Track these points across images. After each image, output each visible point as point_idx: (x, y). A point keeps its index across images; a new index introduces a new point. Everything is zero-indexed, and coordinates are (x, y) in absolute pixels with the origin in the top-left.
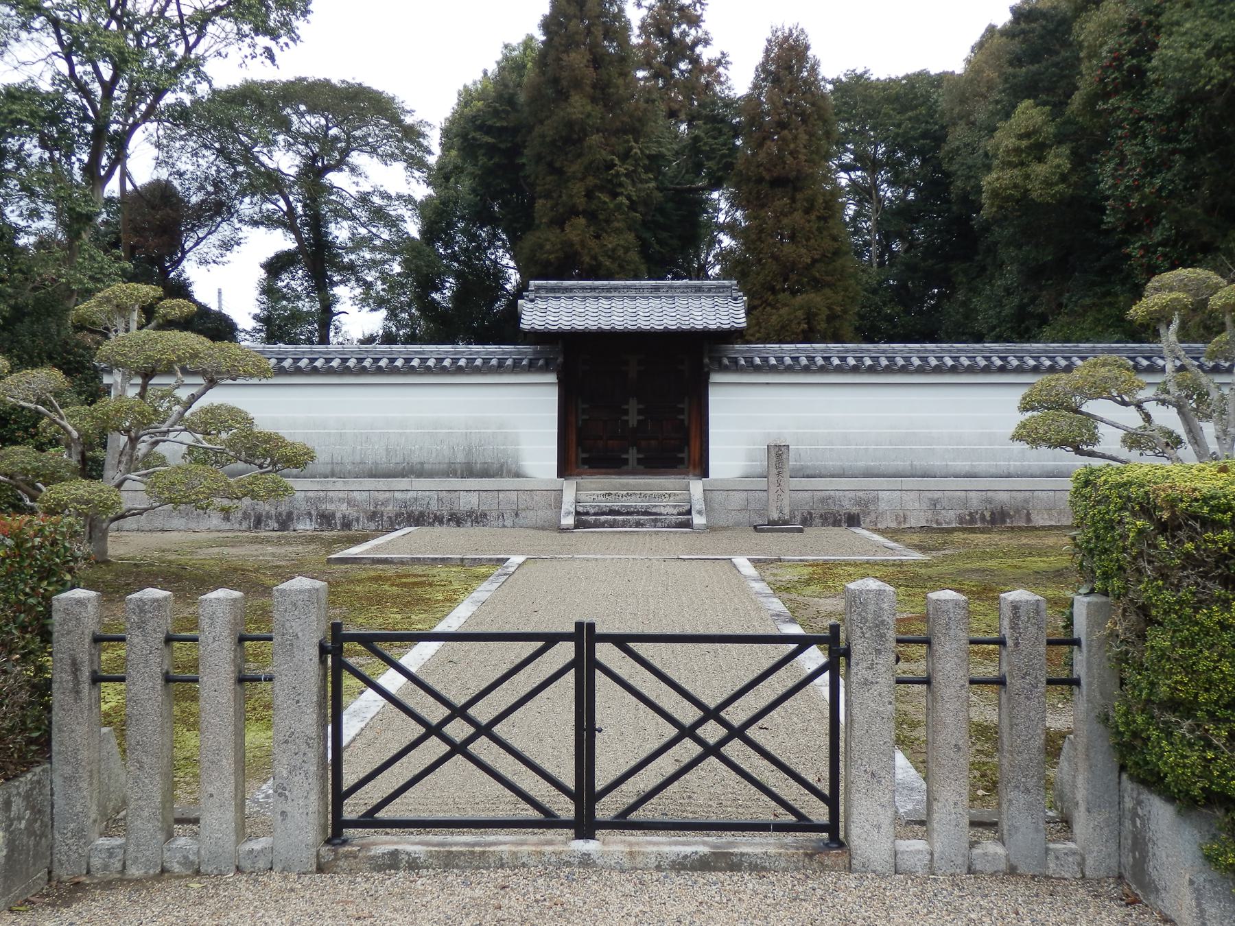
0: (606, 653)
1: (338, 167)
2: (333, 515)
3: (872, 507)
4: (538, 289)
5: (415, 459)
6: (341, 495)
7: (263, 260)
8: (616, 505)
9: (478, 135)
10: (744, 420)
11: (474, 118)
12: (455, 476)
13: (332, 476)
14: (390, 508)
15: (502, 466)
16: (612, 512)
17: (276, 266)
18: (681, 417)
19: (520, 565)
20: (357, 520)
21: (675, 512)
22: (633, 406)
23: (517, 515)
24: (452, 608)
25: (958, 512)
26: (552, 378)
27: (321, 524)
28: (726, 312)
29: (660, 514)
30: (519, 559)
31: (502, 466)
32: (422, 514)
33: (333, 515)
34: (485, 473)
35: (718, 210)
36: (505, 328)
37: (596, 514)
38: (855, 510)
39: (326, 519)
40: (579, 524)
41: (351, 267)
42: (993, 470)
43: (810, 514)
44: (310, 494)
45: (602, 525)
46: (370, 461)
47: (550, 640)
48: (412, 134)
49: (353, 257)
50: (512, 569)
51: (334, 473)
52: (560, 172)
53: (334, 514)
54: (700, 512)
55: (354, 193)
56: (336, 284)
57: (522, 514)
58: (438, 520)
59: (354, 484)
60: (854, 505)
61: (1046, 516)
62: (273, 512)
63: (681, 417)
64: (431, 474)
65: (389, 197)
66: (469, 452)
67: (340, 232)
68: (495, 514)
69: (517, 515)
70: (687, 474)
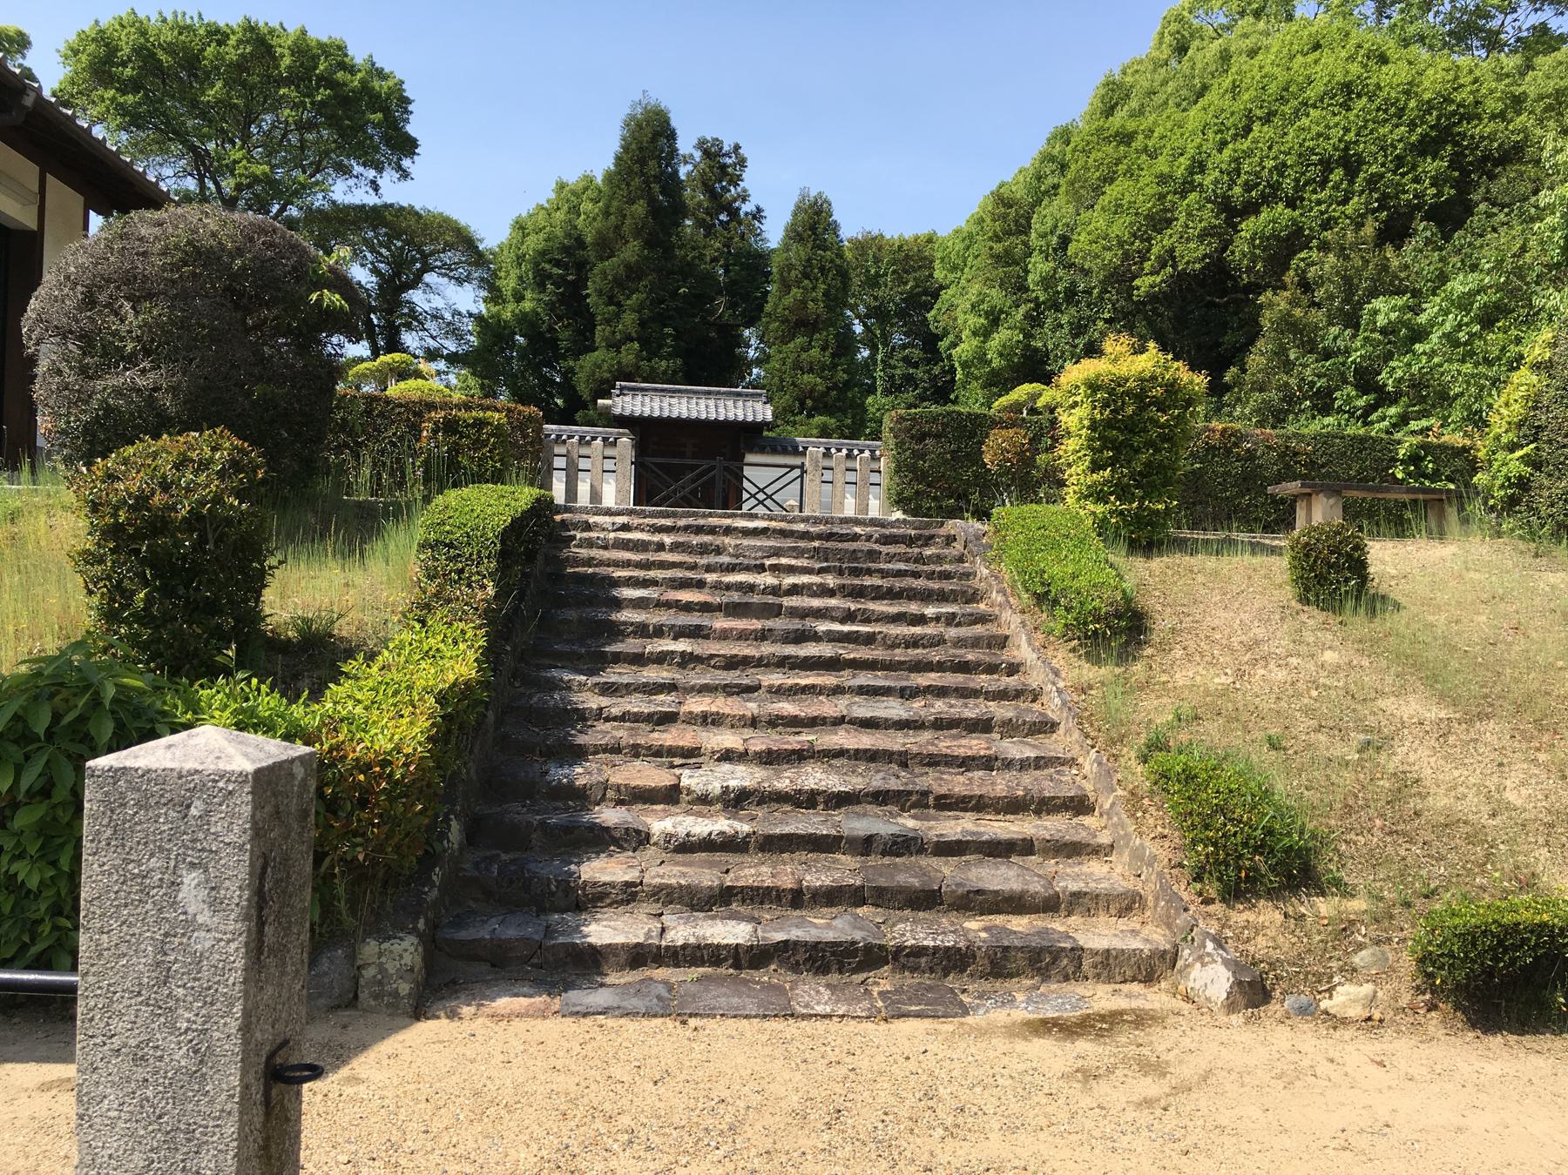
1: (415, 282)
4: (622, 388)
9: (547, 266)
28: (762, 412)
35: (750, 347)
52: (619, 305)
65: (460, 314)
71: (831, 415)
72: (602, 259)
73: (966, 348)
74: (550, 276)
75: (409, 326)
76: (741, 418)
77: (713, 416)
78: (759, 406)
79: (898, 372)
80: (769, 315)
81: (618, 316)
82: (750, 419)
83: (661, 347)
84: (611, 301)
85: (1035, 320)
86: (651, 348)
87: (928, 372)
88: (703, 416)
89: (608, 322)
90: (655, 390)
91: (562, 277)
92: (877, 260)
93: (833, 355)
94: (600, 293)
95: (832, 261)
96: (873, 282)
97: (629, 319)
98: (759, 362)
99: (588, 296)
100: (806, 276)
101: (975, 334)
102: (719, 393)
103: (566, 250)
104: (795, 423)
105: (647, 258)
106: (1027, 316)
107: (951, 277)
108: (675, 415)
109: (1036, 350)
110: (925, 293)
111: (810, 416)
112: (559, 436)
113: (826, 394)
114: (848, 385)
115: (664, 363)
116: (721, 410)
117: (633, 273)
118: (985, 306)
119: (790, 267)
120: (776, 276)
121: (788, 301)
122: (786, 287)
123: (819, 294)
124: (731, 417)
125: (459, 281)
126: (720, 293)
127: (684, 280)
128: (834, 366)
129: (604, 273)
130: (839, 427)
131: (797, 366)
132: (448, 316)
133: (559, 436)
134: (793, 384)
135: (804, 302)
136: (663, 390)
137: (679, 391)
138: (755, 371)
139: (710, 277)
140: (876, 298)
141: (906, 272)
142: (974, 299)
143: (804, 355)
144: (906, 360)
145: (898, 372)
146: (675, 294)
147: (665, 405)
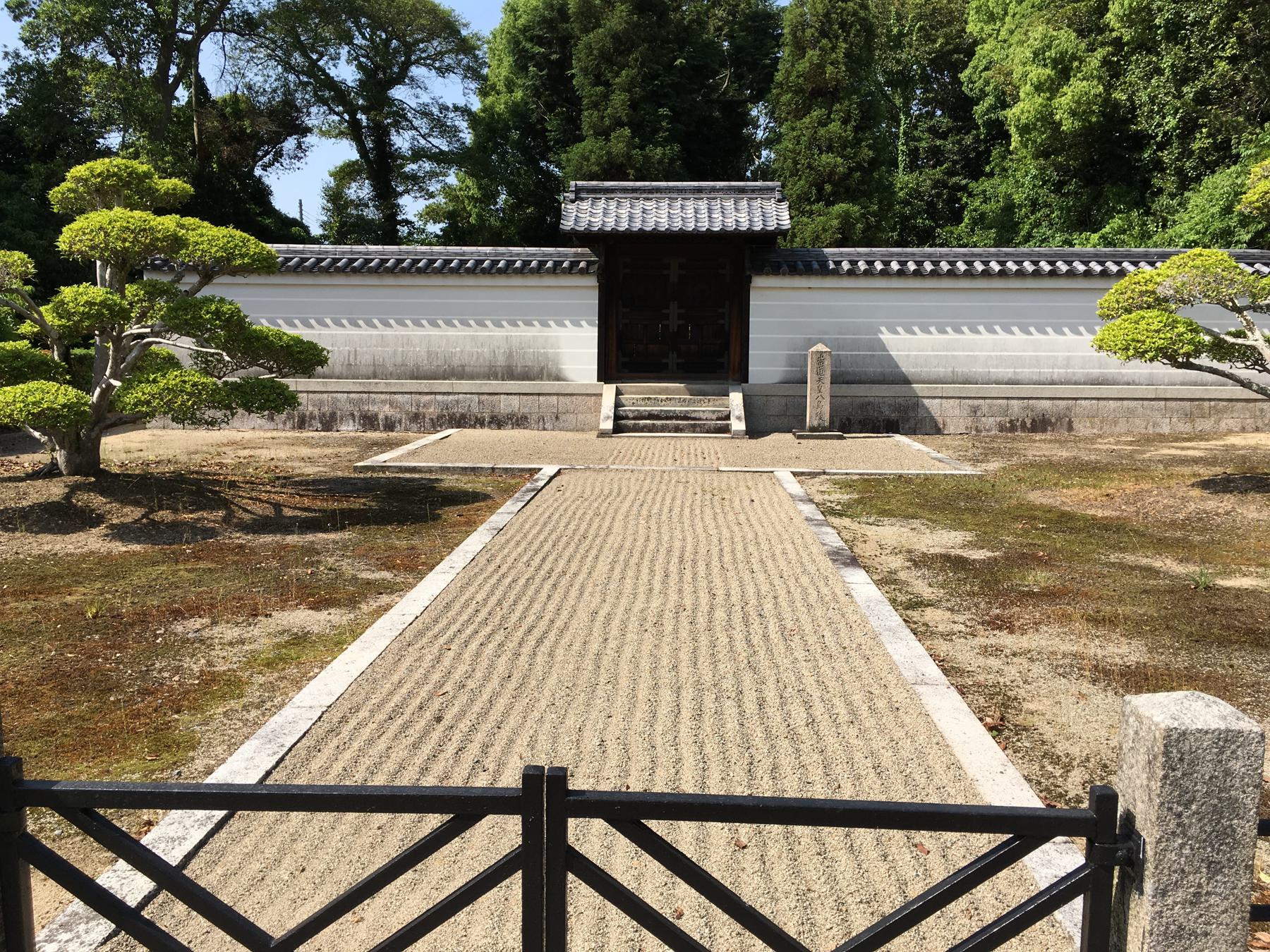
0: (591, 837)
1: (400, 79)
2: (376, 416)
3: (911, 414)
4: (578, 191)
5: (456, 362)
6: (383, 397)
7: (332, 169)
8: (656, 409)
9: (528, 45)
10: (782, 321)
11: (525, 30)
12: (496, 378)
13: (375, 377)
14: (431, 410)
15: (542, 369)
16: (651, 416)
17: (346, 173)
18: (722, 322)
19: (552, 478)
20: (400, 422)
21: (714, 417)
22: (674, 309)
23: (557, 418)
24: (468, 534)
25: (998, 419)
26: (592, 281)
27: (364, 426)
28: (771, 213)
29: (700, 419)
30: (549, 470)
31: (542, 369)
32: (463, 416)
33: (376, 416)
34: (526, 376)
35: (757, 127)
36: (545, 229)
37: (634, 418)
38: (894, 416)
39: (369, 421)
40: (618, 429)
41: (414, 178)
42: (1035, 378)
43: (849, 419)
44: (352, 395)
45: (642, 429)
46: (411, 364)
47: (464, 809)
48: (466, 47)
49: (414, 167)
50: (541, 483)
51: (351, 372)
52: (607, 84)
53: (376, 415)
54: (739, 418)
55: (414, 105)
56: (401, 194)
57: (563, 417)
58: (480, 423)
59: (396, 385)
60: (894, 411)
61: (1088, 424)
62: (316, 412)
63: (722, 322)
64: (472, 377)
65: (447, 108)
66: (510, 355)
67: (402, 141)
68: (535, 417)
69: (557, 418)
70: (726, 379)
71: (854, 200)
72: (586, 31)
73: (1023, 110)
74: (533, 57)
75: (396, 125)
76: (744, 226)
77: (704, 226)
78: (771, 206)
79: (924, 144)
80: (780, 85)
81: (606, 97)
82: (758, 227)
83: (655, 131)
84: (598, 80)
85: (1113, 71)
86: (643, 131)
87: (959, 142)
88: (691, 226)
89: (595, 105)
90: (625, 190)
91: (545, 56)
92: (900, 17)
93: (857, 129)
94: (585, 71)
95: (855, 14)
96: (897, 42)
97: (619, 99)
98: (768, 143)
99: (573, 76)
100: (823, 34)
101: (1038, 88)
102: (713, 190)
103: (549, 23)
104: (811, 213)
105: (637, 25)
106: (1105, 62)
107: (988, 29)
108: (649, 227)
109: (1117, 105)
110: (957, 50)
111: (829, 204)
112: (495, 263)
113: (848, 175)
114: (874, 164)
115: (659, 150)
116: (717, 215)
117: (622, 44)
118: (1052, 53)
119: (804, 25)
120: (788, 38)
121: (803, 66)
122: (800, 48)
123: (840, 55)
124: (731, 225)
125: (442, 72)
126: (723, 65)
127: (681, 49)
128: (857, 142)
129: (589, 47)
130: (863, 215)
131: (814, 140)
132: (435, 111)
133: (495, 263)
134: (810, 166)
135: (820, 67)
136: (634, 190)
137: (658, 190)
138: (764, 153)
139: (713, 47)
140: (898, 62)
141: (933, 27)
142: (1037, 45)
143: (822, 131)
144: (933, 131)
145: (924, 144)
146: (670, 66)
147: (637, 212)
